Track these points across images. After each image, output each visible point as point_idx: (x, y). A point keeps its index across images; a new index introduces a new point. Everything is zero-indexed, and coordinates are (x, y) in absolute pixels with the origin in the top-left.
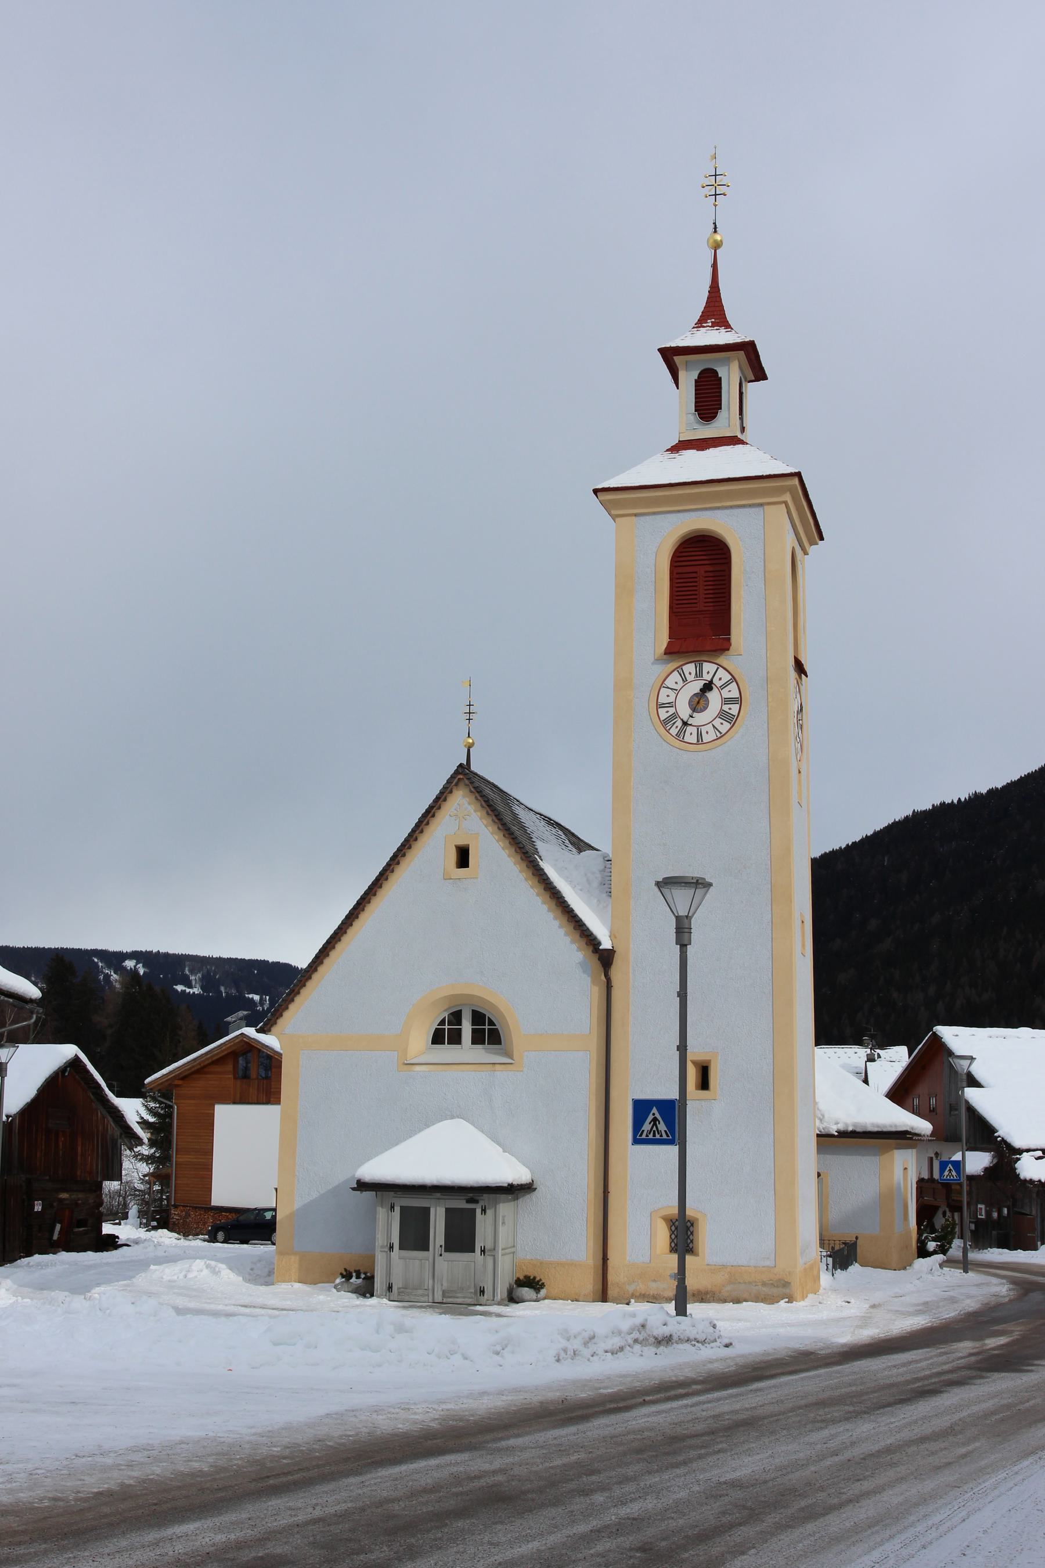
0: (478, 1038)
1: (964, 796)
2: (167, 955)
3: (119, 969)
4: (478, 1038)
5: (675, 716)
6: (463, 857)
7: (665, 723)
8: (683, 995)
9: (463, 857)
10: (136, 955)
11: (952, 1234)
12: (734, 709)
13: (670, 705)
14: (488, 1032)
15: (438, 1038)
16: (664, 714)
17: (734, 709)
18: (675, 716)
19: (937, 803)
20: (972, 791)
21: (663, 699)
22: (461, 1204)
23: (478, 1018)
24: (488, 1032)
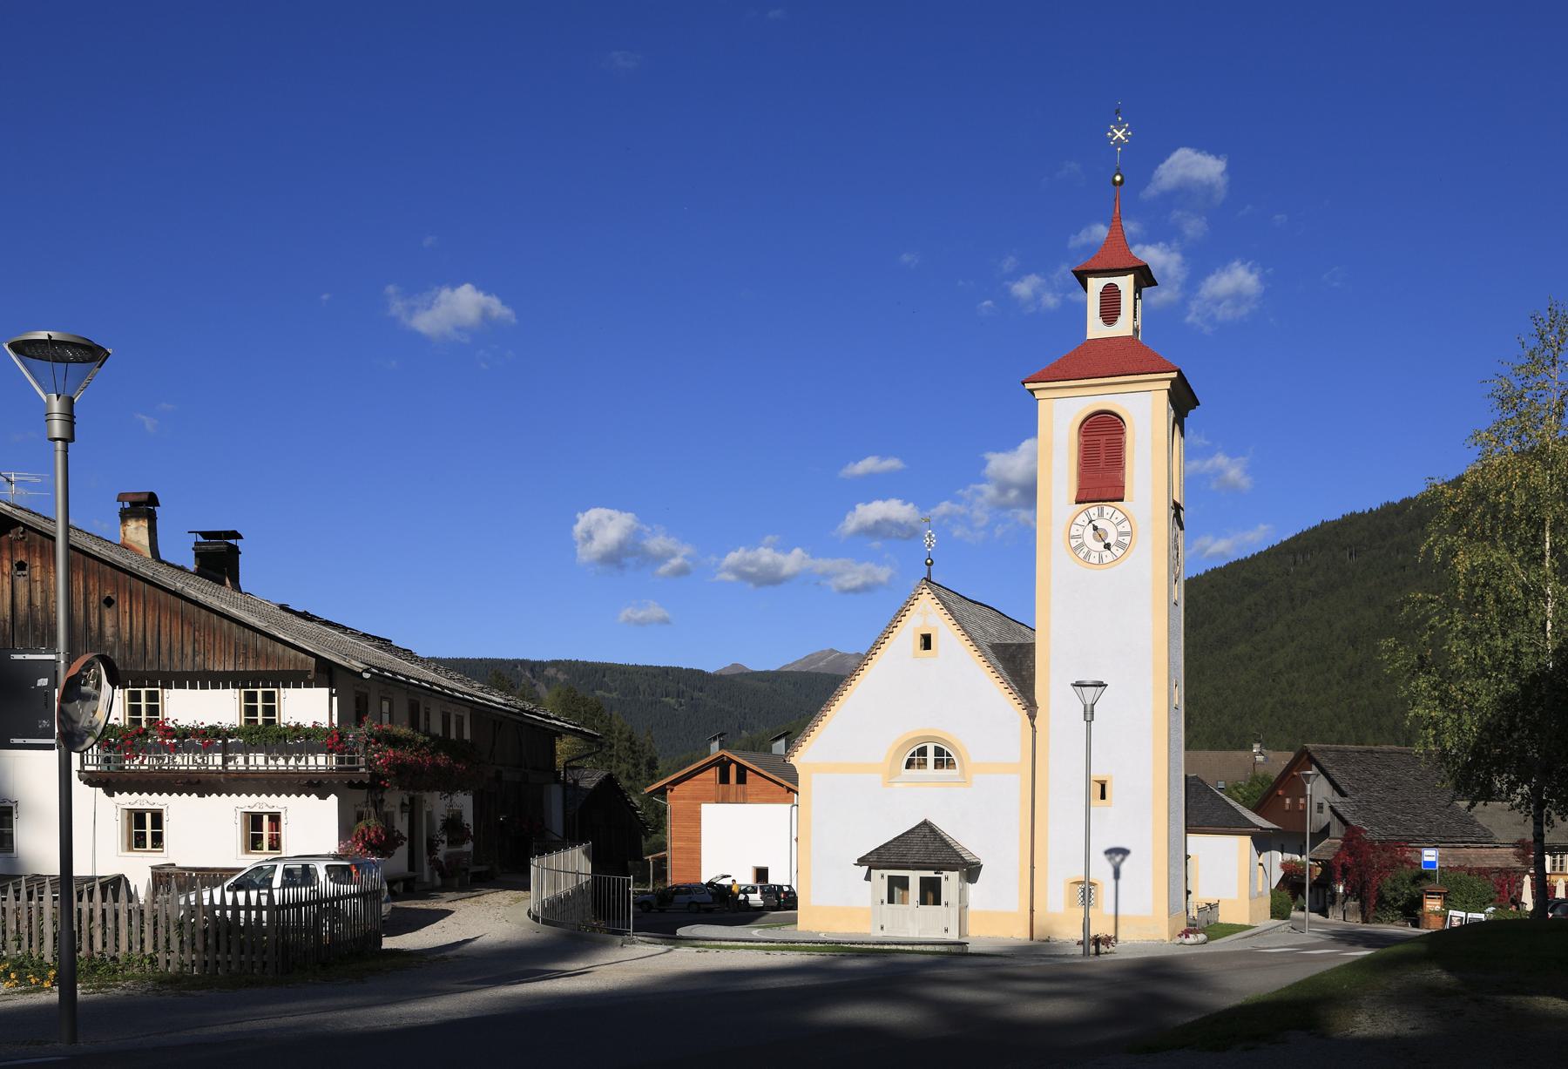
0: (939, 764)
1: (1375, 506)
2: (585, 664)
3: (549, 682)
4: (939, 764)
5: (1082, 544)
6: (927, 642)
7: (1075, 549)
8: (1032, 867)
9: (927, 642)
10: (555, 664)
11: (1372, 902)
12: (1127, 540)
13: (1078, 537)
14: (943, 759)
15: (909, 764)
16: (1074, 543)
17: (1127, 540)
18: (1082, 544)
19: (1348, 512)
20: (1384, 501)
21: (1073, 533)
22: (931, 874)
23: (939, 751)
24: (943, 759)
